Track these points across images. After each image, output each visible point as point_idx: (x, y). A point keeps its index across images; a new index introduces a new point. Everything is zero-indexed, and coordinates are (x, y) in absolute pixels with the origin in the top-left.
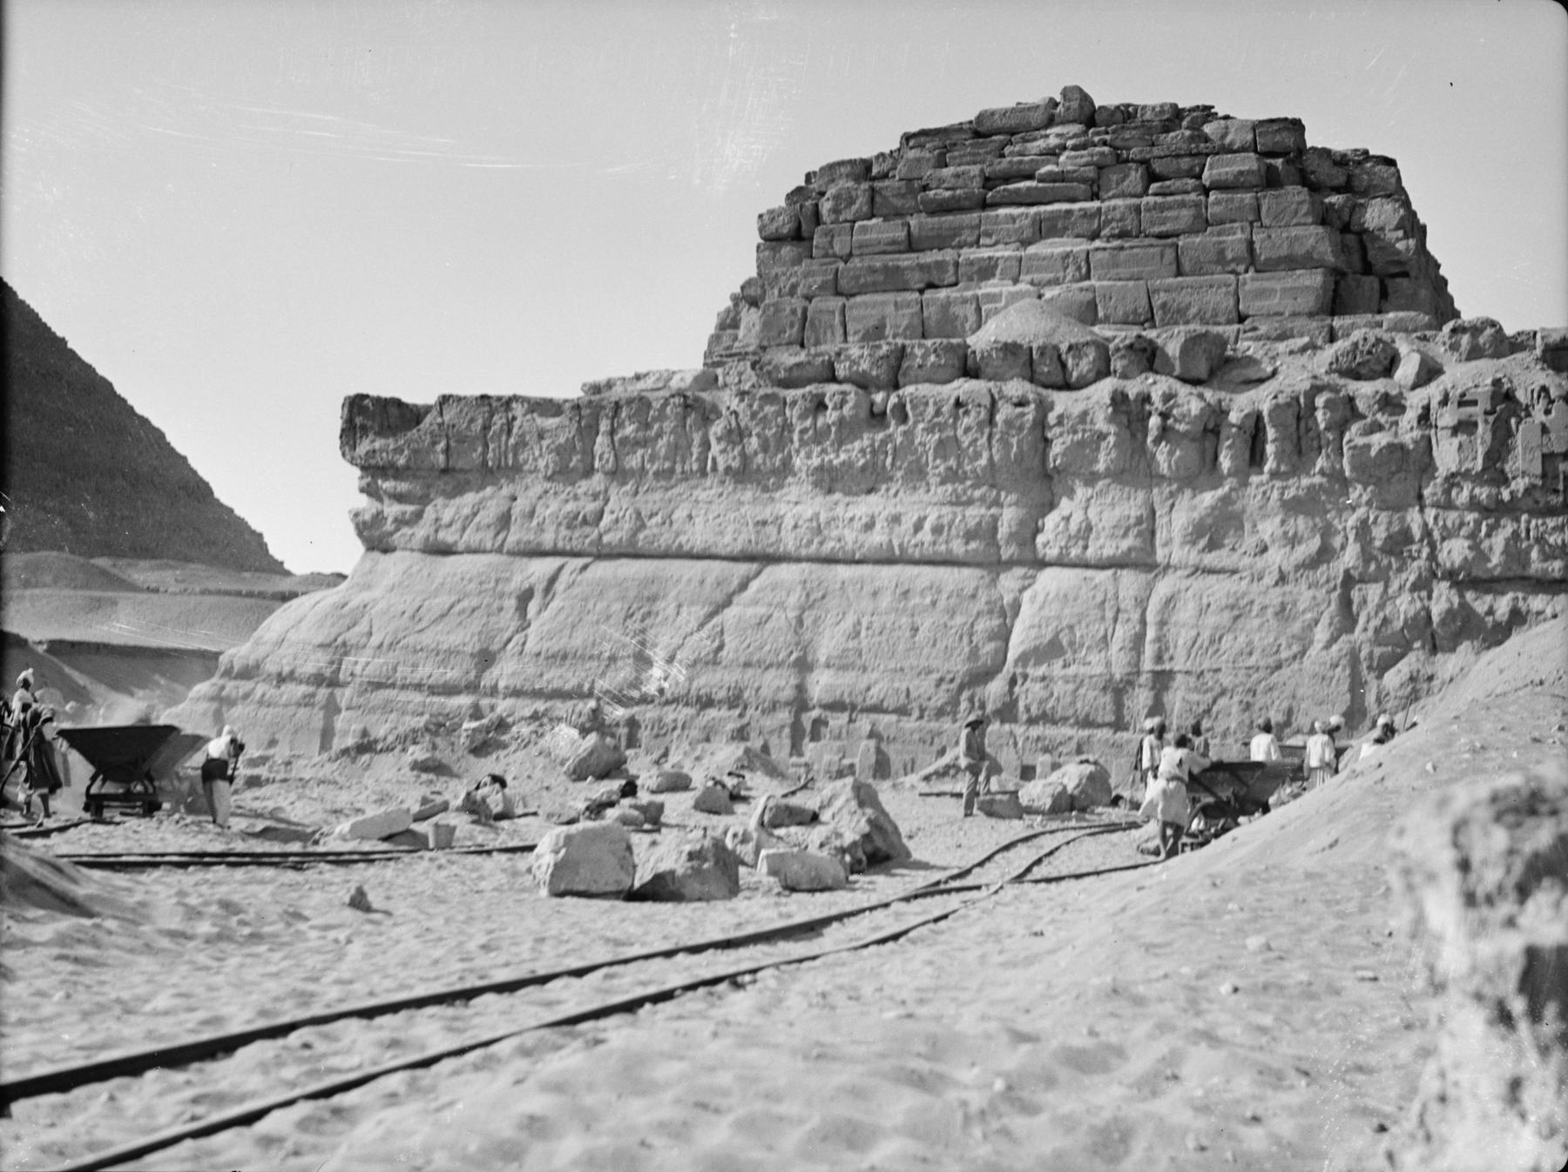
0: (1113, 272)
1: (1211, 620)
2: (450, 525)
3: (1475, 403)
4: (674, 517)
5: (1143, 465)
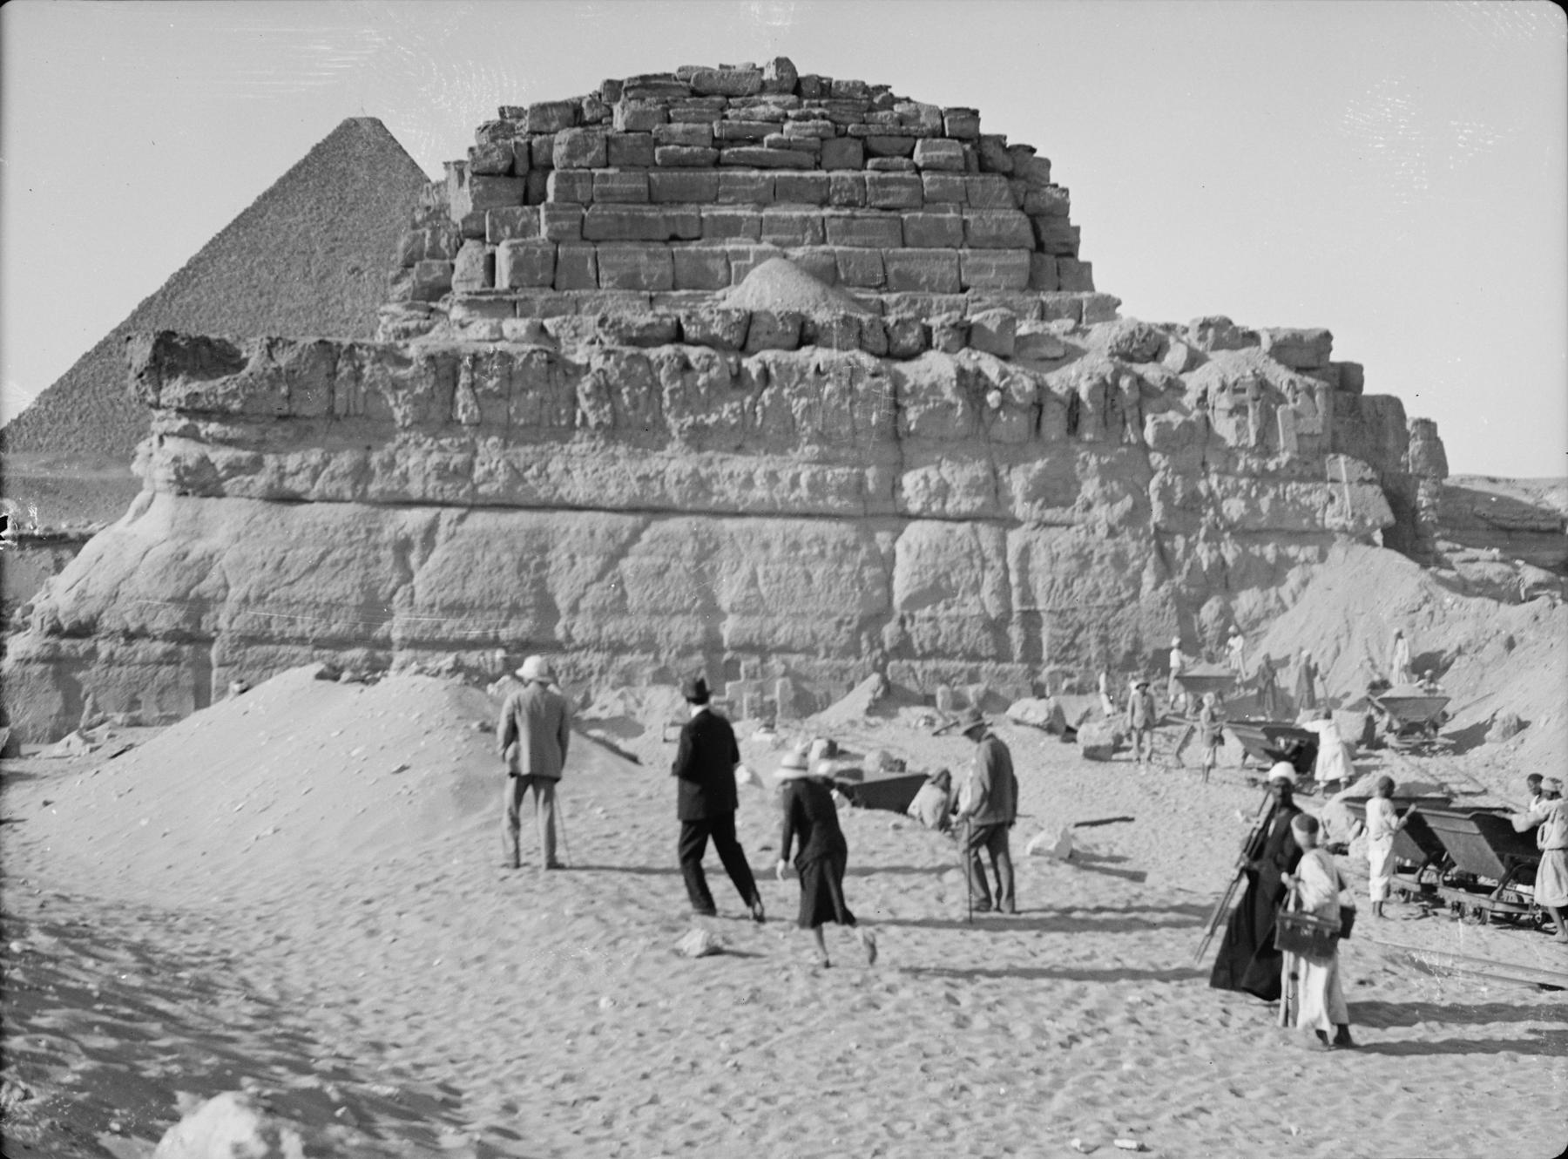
0: (847, 239)
1: (1062, 567)
2: (297, 473)
3: (1244, 391)
4: (550, 469)
5: (981, 432)
